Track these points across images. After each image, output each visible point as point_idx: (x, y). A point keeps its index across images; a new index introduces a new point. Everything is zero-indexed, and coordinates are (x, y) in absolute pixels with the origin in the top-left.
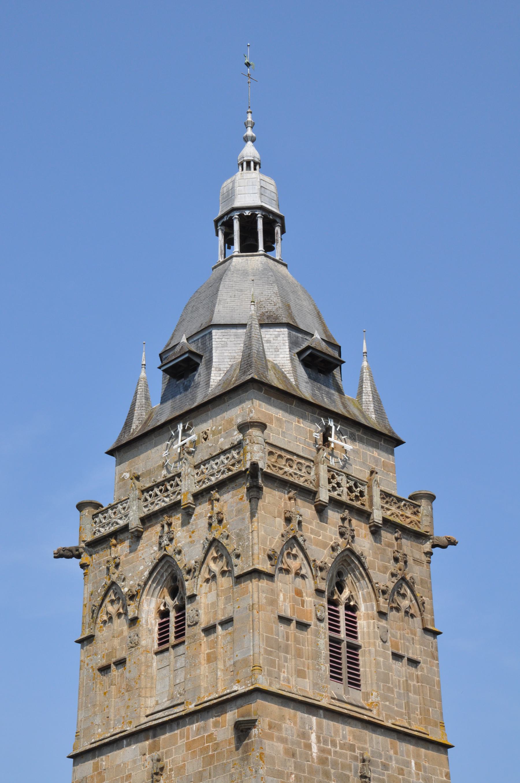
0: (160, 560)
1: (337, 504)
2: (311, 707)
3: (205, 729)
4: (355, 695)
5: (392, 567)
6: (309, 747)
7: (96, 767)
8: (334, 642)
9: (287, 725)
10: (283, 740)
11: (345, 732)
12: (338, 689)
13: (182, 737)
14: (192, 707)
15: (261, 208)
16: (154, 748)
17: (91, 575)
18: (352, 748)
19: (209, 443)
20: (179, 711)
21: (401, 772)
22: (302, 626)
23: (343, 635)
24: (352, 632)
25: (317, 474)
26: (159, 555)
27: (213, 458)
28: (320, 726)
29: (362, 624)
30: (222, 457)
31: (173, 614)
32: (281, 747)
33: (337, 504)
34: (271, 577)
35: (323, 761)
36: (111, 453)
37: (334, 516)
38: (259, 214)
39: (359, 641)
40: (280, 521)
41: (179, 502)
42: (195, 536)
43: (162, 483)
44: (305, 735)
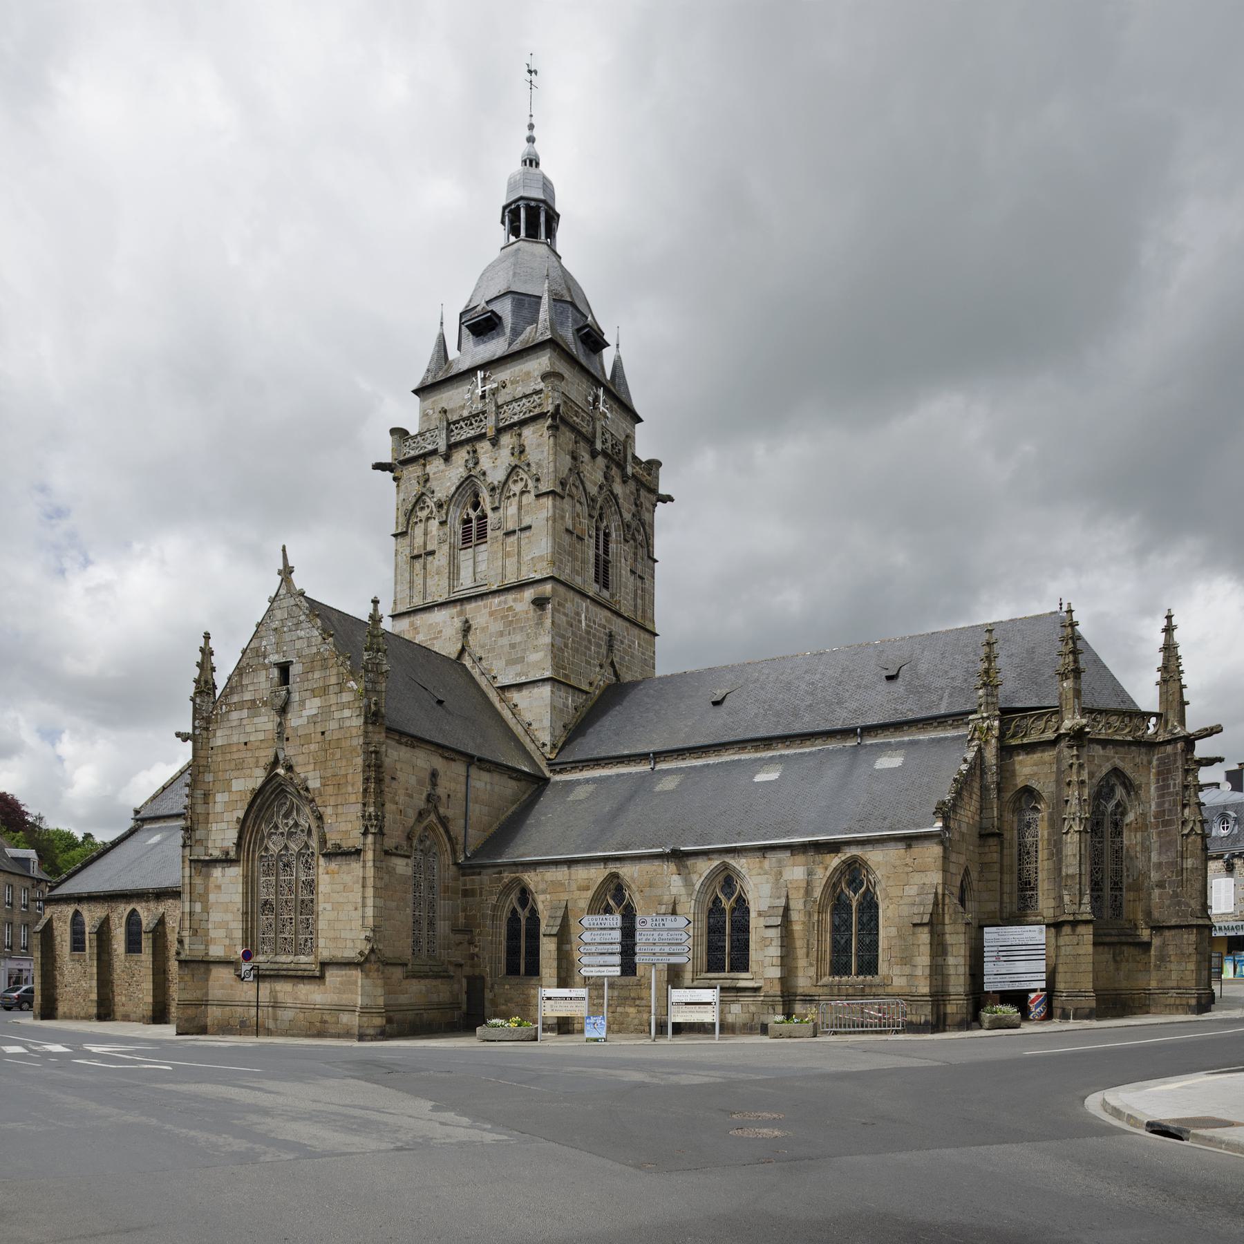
0: (467, 479)
1: (604, 453)
2: (584, 595)
3: (505, 602)
4: (606, 594)
5: (633, 508)
6: (580, 622)
7: (412, 624)
8: (597, 556)
9: (568, 605)
10: (566, 615)
11: (603, 614)
12: (596, 587)
13: (485, 607)
14: (494, 588)
15: (521, 198)
16: (461, 613)
17: (402, 488)
18: (604, 627)
19: (506, 390)
20: (483, 589)
21: (630, 647)
22: (580, 539)
23: (601, 552)
24: (606, 552)
25: (594, 428)
26: (465, 475)
27: (516, 400)
28: (587, 608)
29: (612, 546)
30: (524, 400)
31: (474, 524)
32: (564, 619)
33: (604, 453)
35: (588, 633)
36: (416, 392)
37: (601, 461)
38: (521, 203)
39: (610, 558)
40: (568, 458)
41: (485, 434)
42: (498, 462)
43: (467, 418)
44: (578, 614)
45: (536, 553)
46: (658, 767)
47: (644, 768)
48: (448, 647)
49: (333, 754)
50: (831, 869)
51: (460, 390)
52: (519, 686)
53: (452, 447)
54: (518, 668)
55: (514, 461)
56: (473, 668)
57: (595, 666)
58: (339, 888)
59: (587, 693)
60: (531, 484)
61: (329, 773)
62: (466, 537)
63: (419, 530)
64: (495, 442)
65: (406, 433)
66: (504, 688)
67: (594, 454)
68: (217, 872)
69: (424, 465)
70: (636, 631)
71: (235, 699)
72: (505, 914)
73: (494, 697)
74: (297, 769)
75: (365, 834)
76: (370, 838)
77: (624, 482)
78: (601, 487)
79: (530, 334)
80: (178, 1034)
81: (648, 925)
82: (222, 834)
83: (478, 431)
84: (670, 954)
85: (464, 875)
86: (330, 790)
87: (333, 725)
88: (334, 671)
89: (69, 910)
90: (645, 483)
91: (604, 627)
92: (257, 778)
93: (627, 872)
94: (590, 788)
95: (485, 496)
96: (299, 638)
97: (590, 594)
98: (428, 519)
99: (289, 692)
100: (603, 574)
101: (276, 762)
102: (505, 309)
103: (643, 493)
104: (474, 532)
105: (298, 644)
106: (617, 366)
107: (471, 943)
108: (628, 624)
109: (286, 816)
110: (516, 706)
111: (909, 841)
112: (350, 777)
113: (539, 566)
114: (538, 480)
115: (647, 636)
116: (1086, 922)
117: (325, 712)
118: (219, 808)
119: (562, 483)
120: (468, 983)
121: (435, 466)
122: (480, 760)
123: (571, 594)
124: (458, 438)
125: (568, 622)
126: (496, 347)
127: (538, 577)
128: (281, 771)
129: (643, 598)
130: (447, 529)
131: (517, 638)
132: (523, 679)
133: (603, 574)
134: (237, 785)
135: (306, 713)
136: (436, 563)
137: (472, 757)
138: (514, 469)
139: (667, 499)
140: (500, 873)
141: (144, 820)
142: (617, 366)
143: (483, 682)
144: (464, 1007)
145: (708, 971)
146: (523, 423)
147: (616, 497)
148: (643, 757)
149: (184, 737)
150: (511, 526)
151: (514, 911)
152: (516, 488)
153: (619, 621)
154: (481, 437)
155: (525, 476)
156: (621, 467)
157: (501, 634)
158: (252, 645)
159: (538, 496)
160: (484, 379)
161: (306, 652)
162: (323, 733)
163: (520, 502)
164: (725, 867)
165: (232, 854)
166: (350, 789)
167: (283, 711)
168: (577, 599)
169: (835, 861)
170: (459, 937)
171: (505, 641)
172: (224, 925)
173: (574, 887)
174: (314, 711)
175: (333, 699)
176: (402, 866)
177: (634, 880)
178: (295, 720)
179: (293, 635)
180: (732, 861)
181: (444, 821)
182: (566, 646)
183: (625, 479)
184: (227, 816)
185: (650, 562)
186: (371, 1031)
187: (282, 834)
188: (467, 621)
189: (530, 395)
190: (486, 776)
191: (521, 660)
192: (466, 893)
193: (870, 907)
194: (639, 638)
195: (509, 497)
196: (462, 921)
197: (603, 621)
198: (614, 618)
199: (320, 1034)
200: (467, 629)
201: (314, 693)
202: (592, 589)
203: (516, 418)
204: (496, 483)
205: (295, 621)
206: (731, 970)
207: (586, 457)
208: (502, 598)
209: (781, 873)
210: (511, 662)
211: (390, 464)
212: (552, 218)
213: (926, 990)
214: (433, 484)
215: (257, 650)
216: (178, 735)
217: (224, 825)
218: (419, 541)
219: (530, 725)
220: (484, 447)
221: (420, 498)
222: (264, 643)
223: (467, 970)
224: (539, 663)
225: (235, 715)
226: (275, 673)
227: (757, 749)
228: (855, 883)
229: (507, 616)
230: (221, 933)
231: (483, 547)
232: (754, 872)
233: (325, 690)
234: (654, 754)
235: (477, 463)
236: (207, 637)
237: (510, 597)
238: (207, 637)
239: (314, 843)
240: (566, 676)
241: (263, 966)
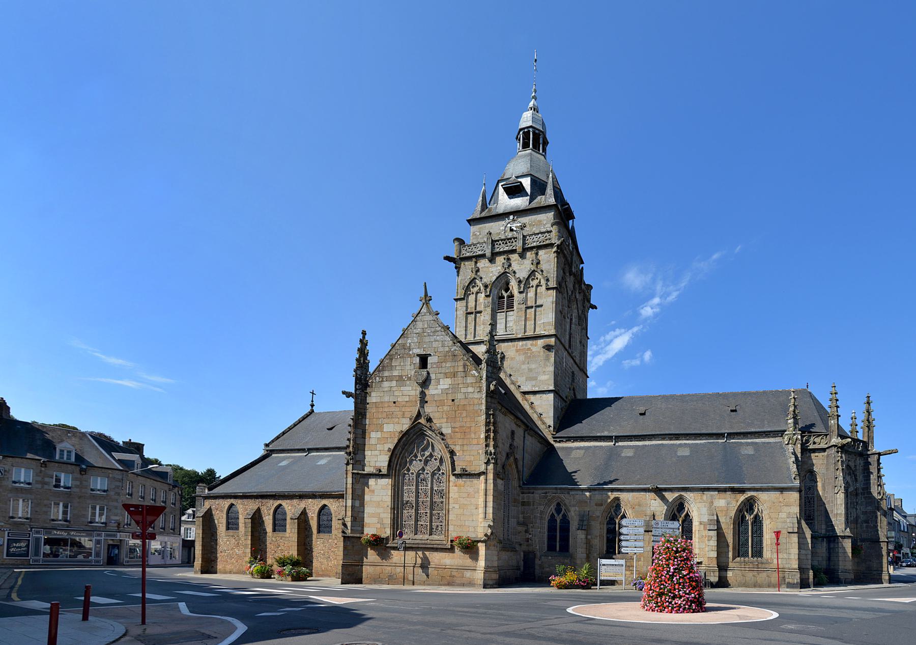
14: (520, 336)
17: (461, 273)
27: (535, 234)
34: (463, 299)
49: (461, 414)
51: (497, 223)
52: (534, 393)
53: (525, 250)
54: (534, 383)
55: (473, 276)
58: (465, 495)
60: (543, 282)
61: (458, 425)
63: (472, 298)
64: (522, 256)
65: (464, 243)
66: (525, 393)
68: (372, 482)
69: (476, 263)
71: (386, 374)
72: (547, 517)
73: (519, 397)
75: (487, 463)
76: (491, 467)
79: (541, 200)
80: (342, 583)
82: (377, 457)
83: (511, 248)
85: (523, 493)
86: (458, 435)
87: (460, 396)
88: (461, 363)
89: (226, 503)
92: (405, 425)
94: (582, 452)
95: (513, 284)
96: (435, 341)
98: (477, 293)
99: (428, 373)
101: (419, 415)
102: (526, 183)
105: (435, 345)
107: (526, 531)
109: (424, 450)
110: (532, 403)
111: (782, 490)
112: (473, 429)
113: (547, 328)
114: (548, 280)
116: (849, 537)
117: (455, 388)
118: (373, 441)
120: (524, 556)
121: (483, 264)
124: (498, 250)
126: (520, 202)
127: (547, 333)
128: (422, 421)
131: (533, 366)
132: (537, 389)
134: (388, 428)
135: (440, 387)
136: (482, 318)
138: (533, 273)
139: (594, 307)
141: (272, 451)
143: (512, 388)
144: (522, 568)
146: (539, 247)
148: (609, 438)
149: (348, 395)
151: (552, 516)
154: (513, 251)
155: (539, 277)
158: (400, 342)
160: (514, 220)
161: (441, 349)
162: (453, 400)
164: (681, 497)
165: (384, 471)
166: (473, 436)
167: (425, 383)
169: (742, 498)
170: (520, 528)
171: (524, 367)
172: (377, 515)
174: (447, 387)
175: (459, 380)
178: (431, 391)
179: (432, 339)
180: (688, 495)
181: (516, 460)
184: (379, 447)
186: (491, 582)
187: (420, 460)
191: (535, 379)
192: (523, 504)
193: (758, 521)
196: (521, 519)
199: (450, 584)
201: (446, 375)
203: (535, 244)
205: (433, 330)
208: (524, 342)
210: (529, 379)
212: (546, 143)
213: (797, 566)
214: (481, 274)
215: (404, 346)
216: (344, 393)
217: (377, 453)
218: (471, 304)
220: (514, 257)
221: (473, 281)
222: (409, 341)
223: (524, 548)
225: (386, 384)
226: (417, 360)
228: (751, 509)
230: (375, 520)
231: (511, 313)
233: (454, 375)
236: (364, 333)
237: (529, 342)
238: (364, 333)
239: (446, 467)
241: (407, 541)
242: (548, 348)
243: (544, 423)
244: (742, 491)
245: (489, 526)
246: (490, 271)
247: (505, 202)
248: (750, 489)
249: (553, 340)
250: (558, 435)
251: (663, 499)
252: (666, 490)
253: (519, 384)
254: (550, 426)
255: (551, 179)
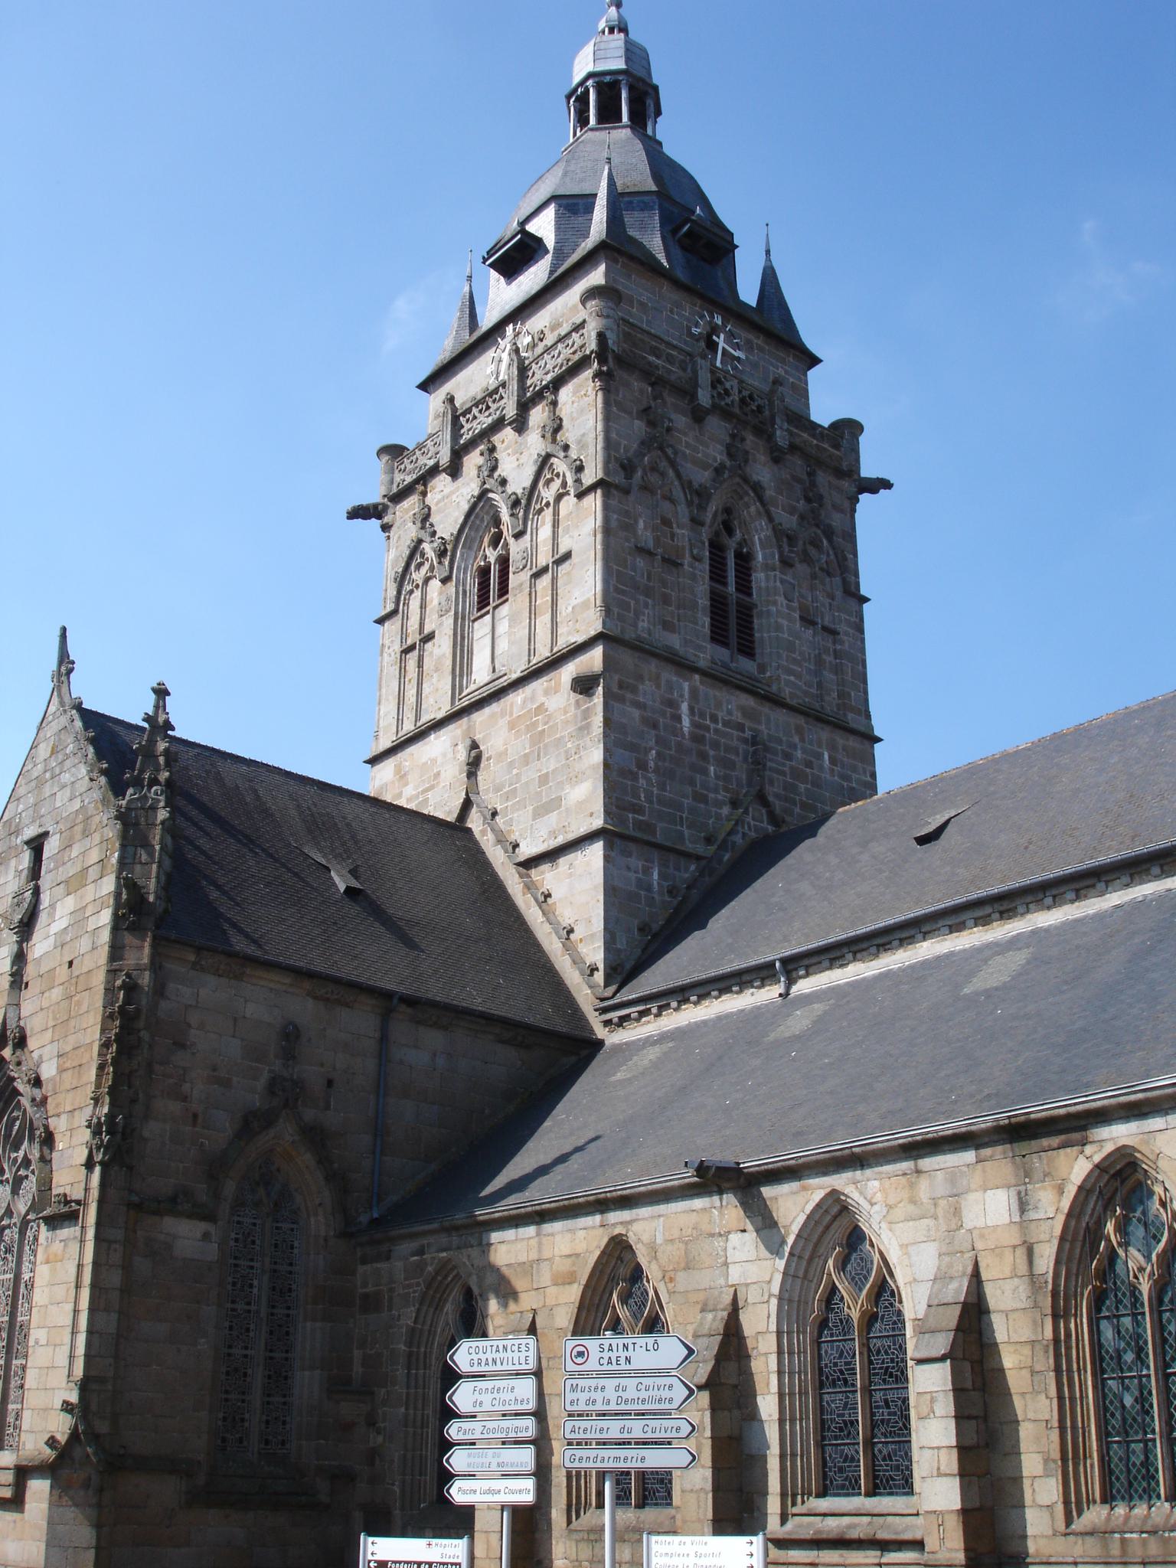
2: (683, 665)
3: (533, 699)
11: (733, 704)
13: (503, 714)
18: (741, 728)
21: (809, 764)
28: (694, 693)
32: (636, 713)
35: (697, 739)
44: (673, 704)
45: (580, 599)
46: (795, 989)
47: (770, 993)
48: (443, 805)
50: (1071, 1191)
52: (551, 856)
53: (524, 406)
56: (483, 833)
57: (719, 804)
59: (698, 858)
62: (483, 601)
66: (530, 863)
67: (698, 416)
69: (424, 494)
70: (825, 734)
74: (32, 1043)
77: (777, 460)
78: (719, 471)
81: (592, 1364)
84: (644, 1443)
90: (831, 466)
91: (741, 728)
93: (646, 1227)
97: (702, 664)
100: (733, 623)
103: (823, 478)
104: (490, 588)
106: (770, 281)
108: (801, 720)
114: (580, 469)
115: (853, 742)
119: (623, 467)
122: (410, 1001)
123: (652, 666)
125: (645, 721)
129: (837, 670)
130: (451, 587)
133: (733, 623)
137: (387, 995)
138: (545, 461)
139: (880, 485)
140: (421, 1252)
142: (770, 281)
145: (823, 1493)
147: (757, 488)
148: (762, 974)
150: (544, 558)
152: (548, 494)
153: (780, 716)
154: (498, 425)
156: (763, 432)
157: (526, 760)
159: (580, 496)
163: (556, 513)
168: (668, 675)
171: (531, 774)
173: (545, 1278)
176: (187, 1237)
177: (653, 1249)
180: (853, 1186)
182: (642, 765)
183: (777, 457)
185: (852, 603)
188: (474, 745)
189: (568, 335)
190: (434, 1039)
191: (554, 804)
194: (832, 747)
195: (541, 510)
197: (737, 716)
198: (766, 709)
200: (474, 764)
202: (707, 654)
204: (519, 492)
206: (872, 1493)
207: (681, 421)
209: (957, 1212)
210: (541, 811)
211: (376, 506)
219: (571, 931)
224: (584, 802)
227: (984, 921)
229: (535, 725)
232: (899, 1213)
234: (785, 961)
235: (494, 469)
240: (648, 827)
242: (583, 685)
243: (577, 960)
244: (1074, 1126)
245: (67, 1407)
246: (448, 501)
247: (501, 295)
248: (1102, 1116)
249: (597, 654)
250: (626, 995)
251: (765, 1222)
252: (776, 1175)
253: (512, 838)
254: (593, 970)
255: (604, 184)
